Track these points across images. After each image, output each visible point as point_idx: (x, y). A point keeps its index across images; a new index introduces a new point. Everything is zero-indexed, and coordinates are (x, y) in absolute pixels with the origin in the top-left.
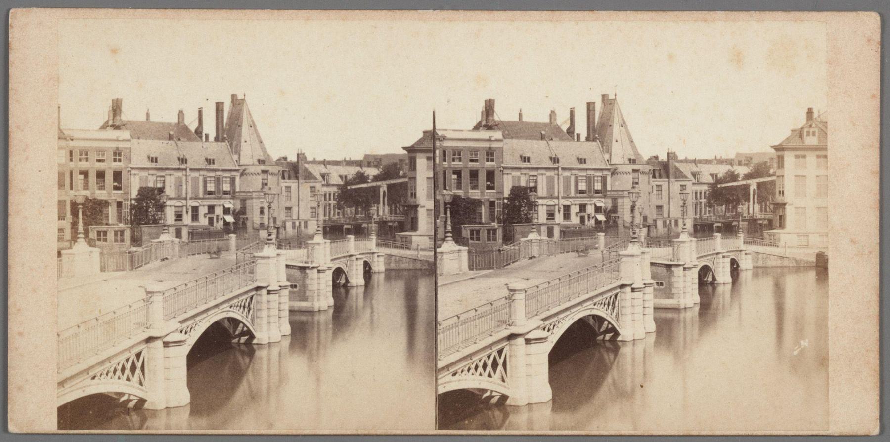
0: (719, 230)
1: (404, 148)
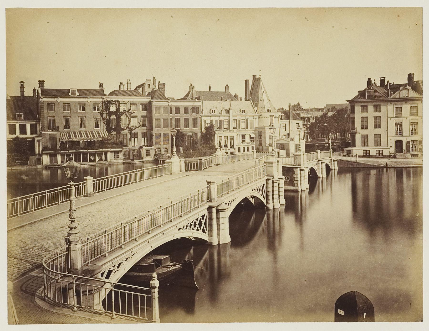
0: (318, 147)
1: (347, 101)
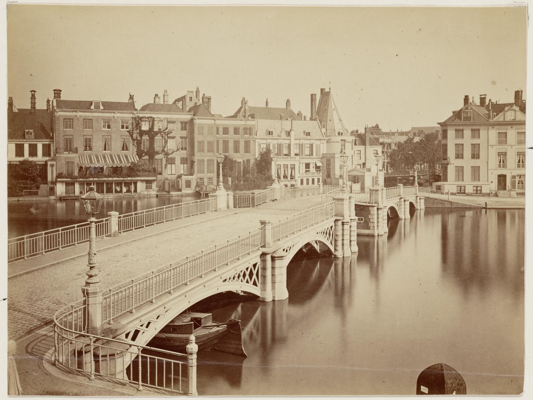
0: (401, 181)
1: (439, 124)
